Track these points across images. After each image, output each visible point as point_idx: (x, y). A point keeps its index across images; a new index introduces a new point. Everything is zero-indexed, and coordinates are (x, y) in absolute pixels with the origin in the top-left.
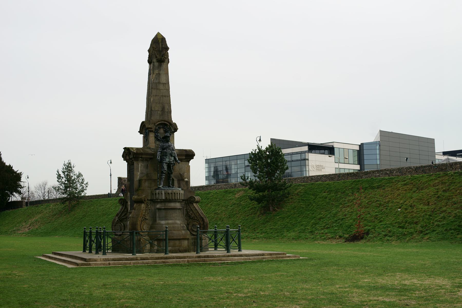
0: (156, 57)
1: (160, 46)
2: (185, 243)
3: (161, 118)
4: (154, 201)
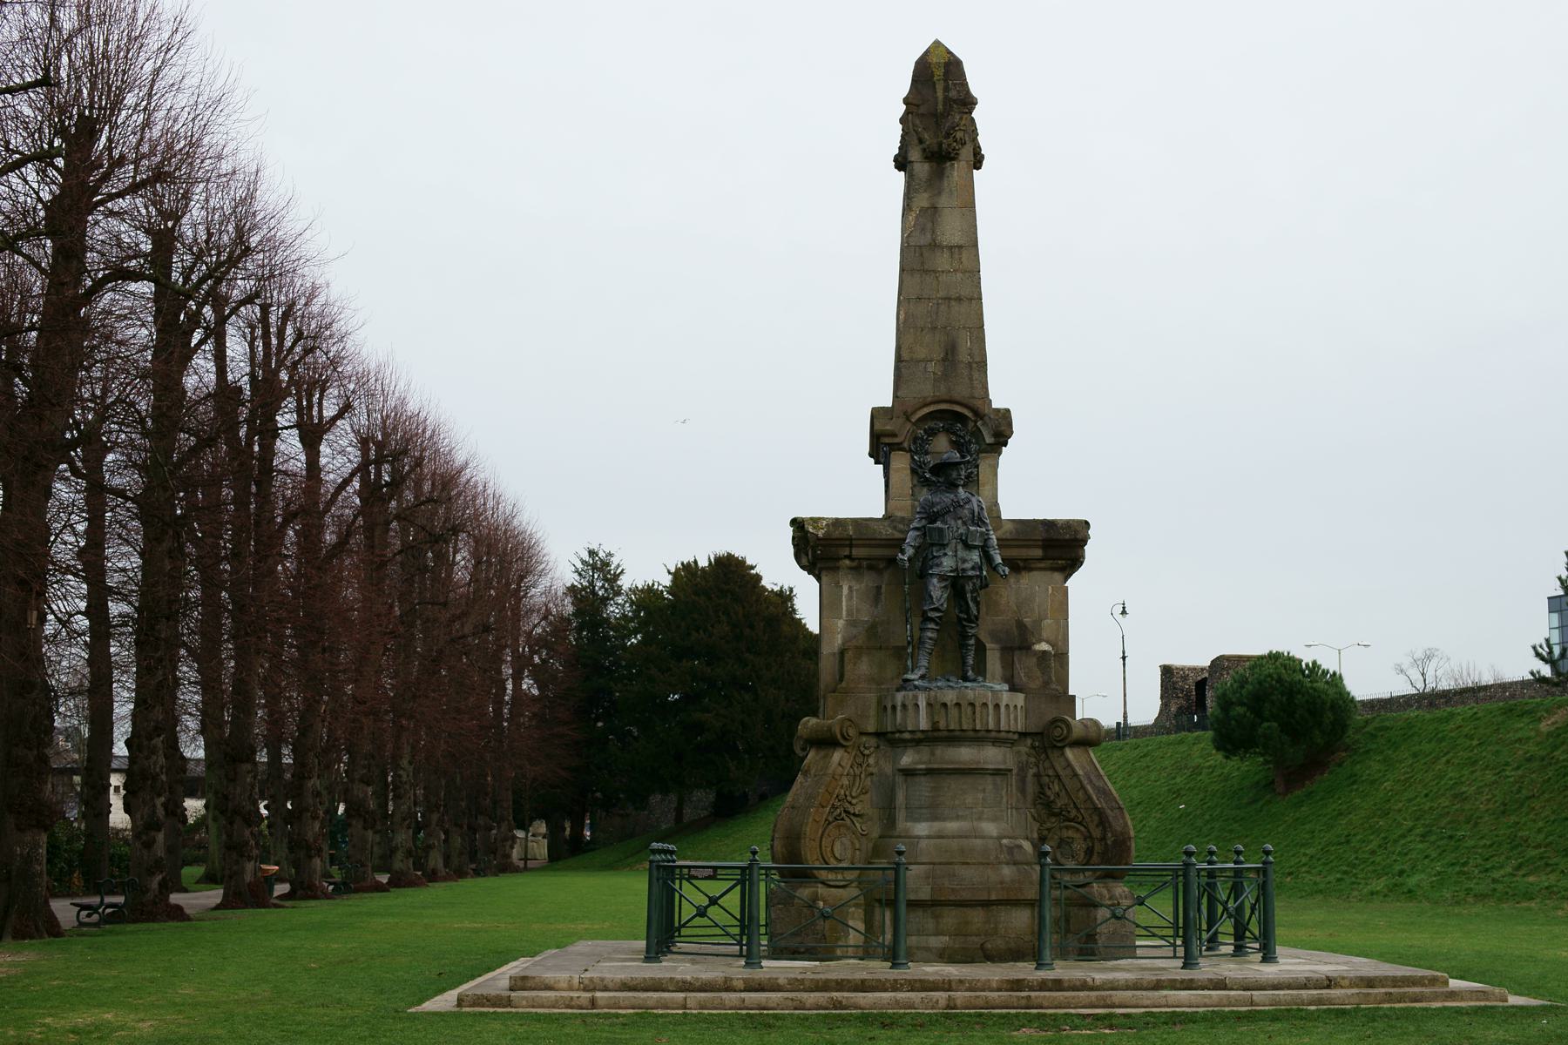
0: (921, 141)
1: (940, 94)
2: (1020, 919)
3: (942, 392)
4: (890, 739)
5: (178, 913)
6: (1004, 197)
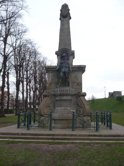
5: (5, 116)
6: (74, 25)
